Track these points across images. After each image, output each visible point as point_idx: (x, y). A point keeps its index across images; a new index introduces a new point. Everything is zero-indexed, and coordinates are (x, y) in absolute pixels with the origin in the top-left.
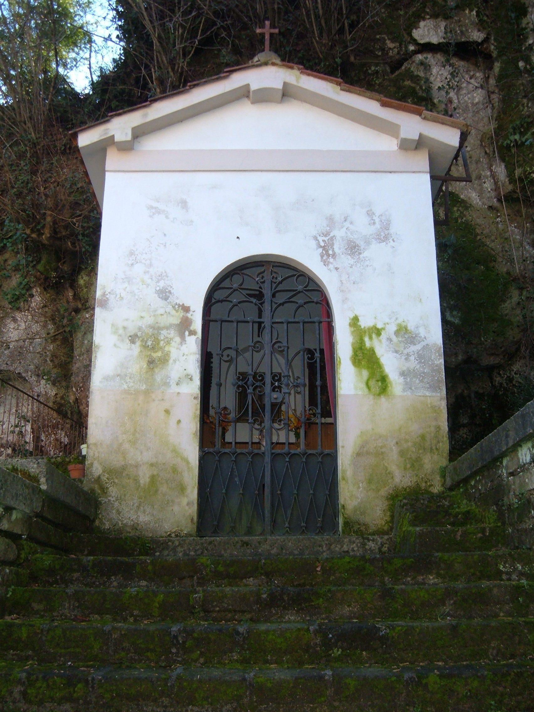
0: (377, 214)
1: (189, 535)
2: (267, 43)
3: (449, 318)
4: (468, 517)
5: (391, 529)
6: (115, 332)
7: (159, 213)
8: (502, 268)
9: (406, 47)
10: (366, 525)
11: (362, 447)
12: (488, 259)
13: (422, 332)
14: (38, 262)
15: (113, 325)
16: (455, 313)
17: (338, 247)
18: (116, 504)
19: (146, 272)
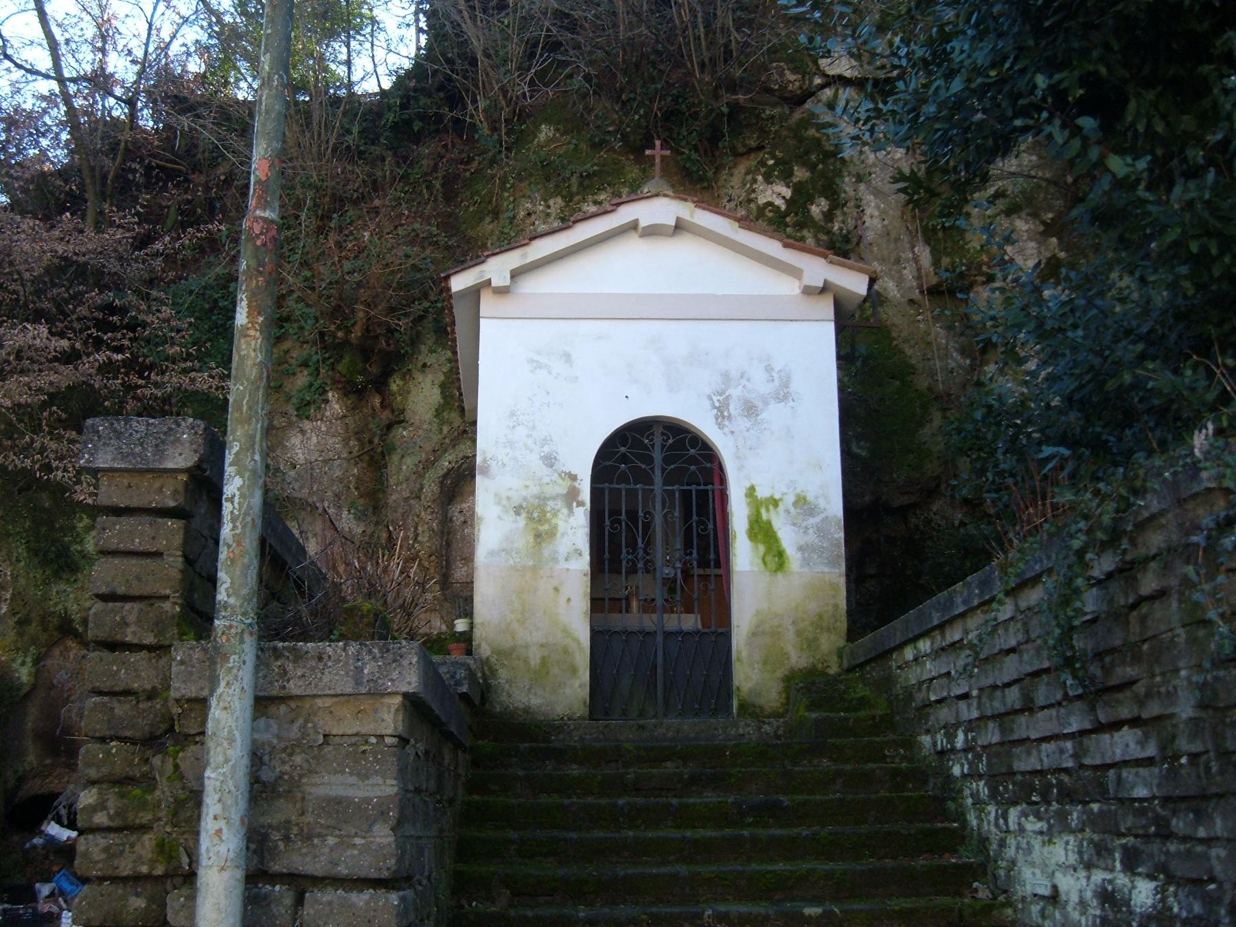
0: (777, 369)
1: (582, 718)
2: (657, 167)
3: (855, 449)
4: (863, 703)
5: (787, 711)
6: (499, 503)
7: (541, 367)
8: (923, 383)
9: (811, 81)
10: (761, 708)
11: (758, 626)
12: (905, 372)
13: (822, 503)
14: (338, 361)
15: (496, 495)
16: (862, 443)
17: (734, 408)
18: (507, 686)
19: (529, 436)
